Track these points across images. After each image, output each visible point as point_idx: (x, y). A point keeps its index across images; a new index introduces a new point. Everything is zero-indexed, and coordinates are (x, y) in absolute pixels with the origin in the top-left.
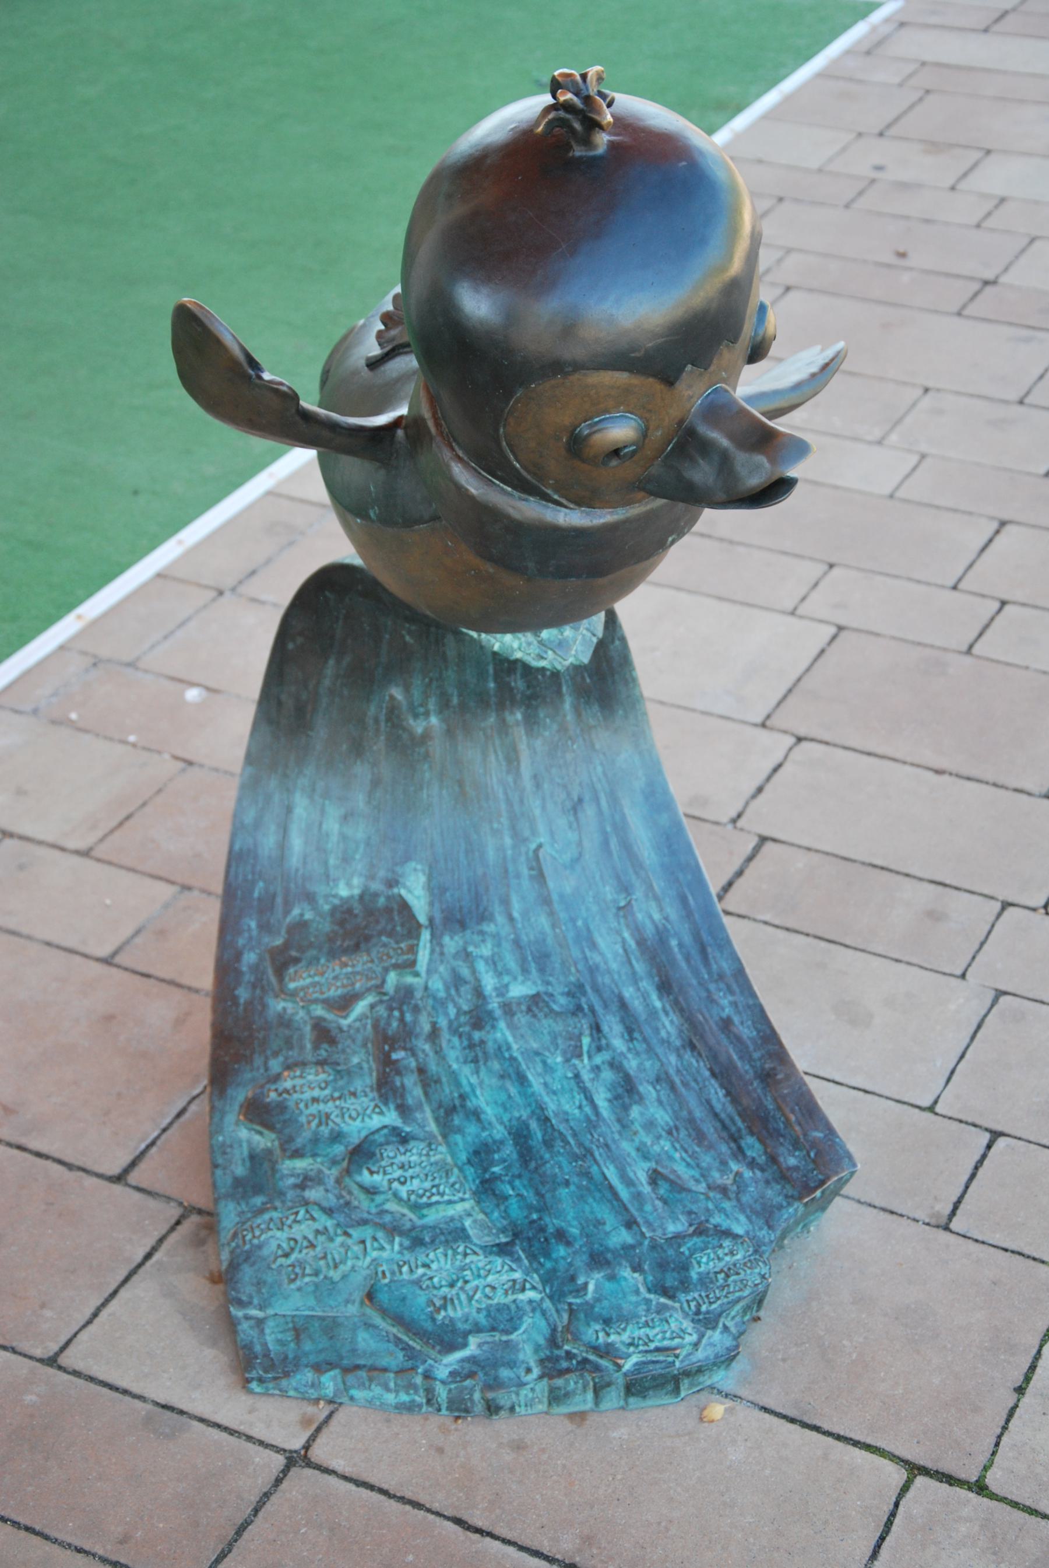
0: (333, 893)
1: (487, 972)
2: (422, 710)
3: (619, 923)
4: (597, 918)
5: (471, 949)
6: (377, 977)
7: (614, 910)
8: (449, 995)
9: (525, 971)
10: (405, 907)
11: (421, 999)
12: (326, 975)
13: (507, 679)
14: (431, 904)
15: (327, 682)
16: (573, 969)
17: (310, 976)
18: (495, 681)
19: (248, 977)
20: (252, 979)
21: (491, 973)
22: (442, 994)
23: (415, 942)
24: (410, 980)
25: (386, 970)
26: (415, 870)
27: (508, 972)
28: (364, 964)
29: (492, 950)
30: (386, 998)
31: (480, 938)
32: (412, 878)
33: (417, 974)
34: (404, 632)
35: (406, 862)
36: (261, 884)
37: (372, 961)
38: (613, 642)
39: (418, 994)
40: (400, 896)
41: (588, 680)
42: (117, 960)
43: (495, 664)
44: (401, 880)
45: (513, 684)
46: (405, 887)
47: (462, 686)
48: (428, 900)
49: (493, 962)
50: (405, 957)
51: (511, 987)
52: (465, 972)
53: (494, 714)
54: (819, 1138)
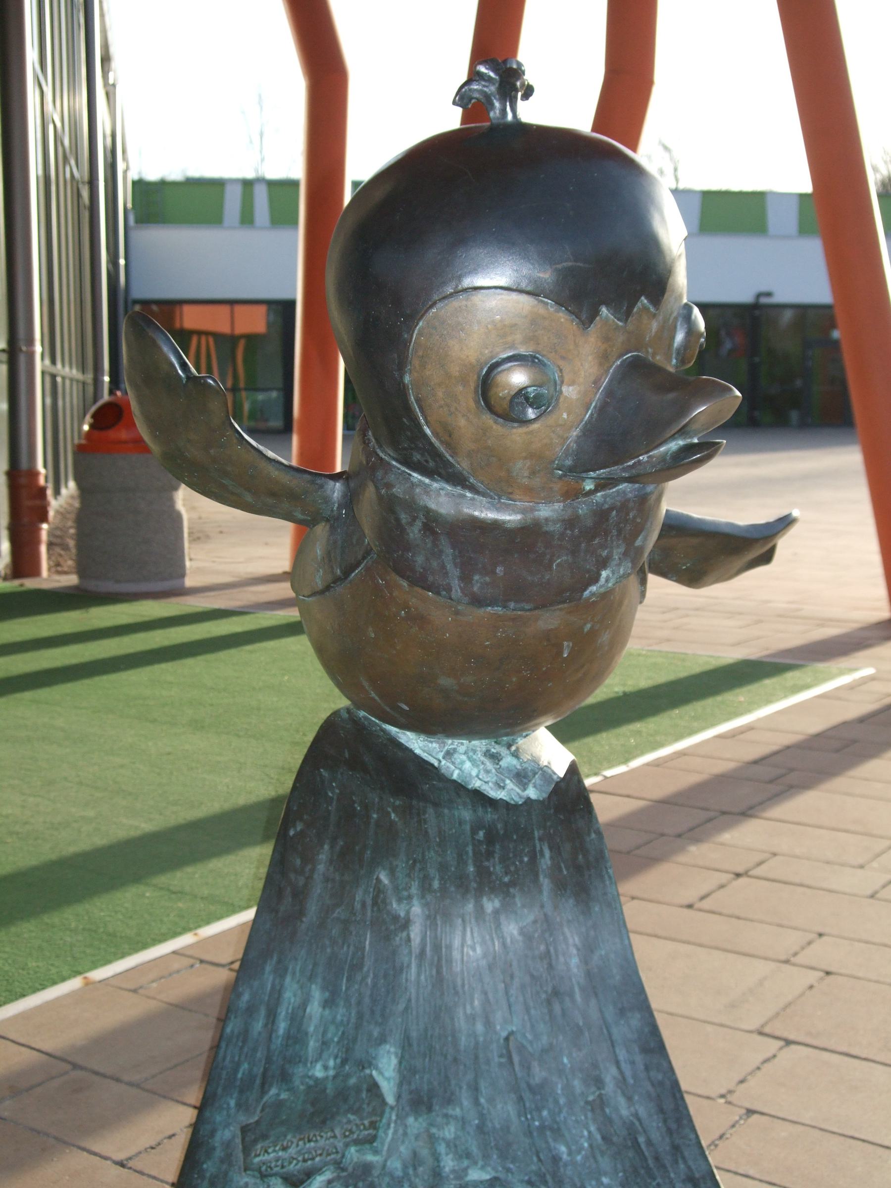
0: (310, 1074)
1: (447, 1154)
2: (405, 893)
3: (586, 1117)
4: (565, 1110)
5: (434, 1130)
6: (337, 1152)
7: (582, 1103)
8: (406, 1174)
9: (486, 1157)
10: (374, 1088)
11: (378, 1177)
12: (290, 1151)
13: (486, 864)
14: (400, 1085)
15: (321, 868)
16: (535, 1159)
17: (274, 1151)
18: (475, 865)
19: (219, 1153)
20: (222, 1154)
21: (451, 1156)
22: (399, 1173)
23: (378, 1119)
24: (370, 1158)
25: (347, 1145)
26: (389, 1052)
27: (468, 1155)
28: (327, 1139)
29: (455, 1133)
30: (345, 1174)
31: (445, 1120)
32: (385, 1060)
33: (376, 1152)
34: (389, 809)
35: (380, 1044)
36: (246, 1066)
37: (335, 1137)
38: (589, 834)
39: (376, 1173)
40: (371, 1076)
41: (565, 873)
42: (131, 1164)
43: (474, 845)
44: (374, 1062)
45: (492, 869)
46: (377, 1068)
47: (443, 868)
48: (397, 1081)
49: (452, 1145)
50: (366, 1132)
51: (470, 1172)
52: (425, 1152)
53: (472, 901)
54: (646, 298)
